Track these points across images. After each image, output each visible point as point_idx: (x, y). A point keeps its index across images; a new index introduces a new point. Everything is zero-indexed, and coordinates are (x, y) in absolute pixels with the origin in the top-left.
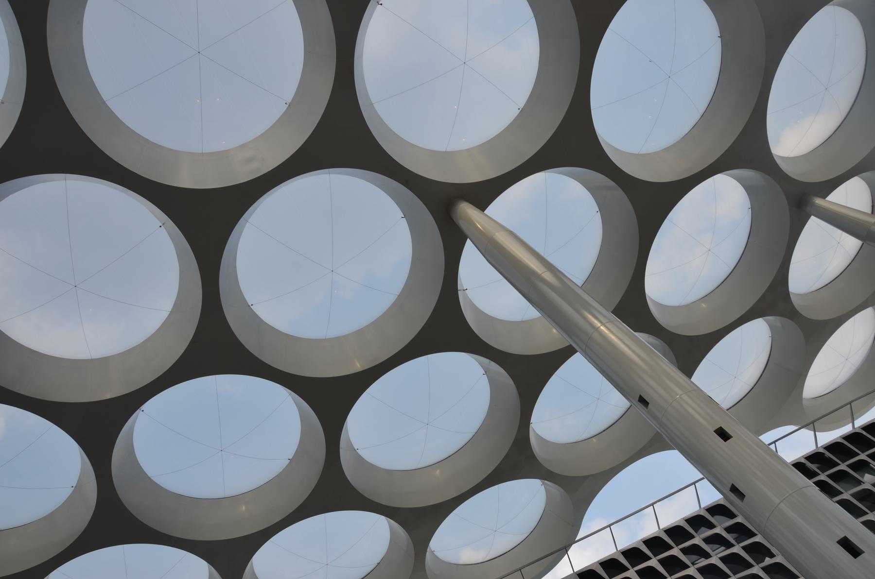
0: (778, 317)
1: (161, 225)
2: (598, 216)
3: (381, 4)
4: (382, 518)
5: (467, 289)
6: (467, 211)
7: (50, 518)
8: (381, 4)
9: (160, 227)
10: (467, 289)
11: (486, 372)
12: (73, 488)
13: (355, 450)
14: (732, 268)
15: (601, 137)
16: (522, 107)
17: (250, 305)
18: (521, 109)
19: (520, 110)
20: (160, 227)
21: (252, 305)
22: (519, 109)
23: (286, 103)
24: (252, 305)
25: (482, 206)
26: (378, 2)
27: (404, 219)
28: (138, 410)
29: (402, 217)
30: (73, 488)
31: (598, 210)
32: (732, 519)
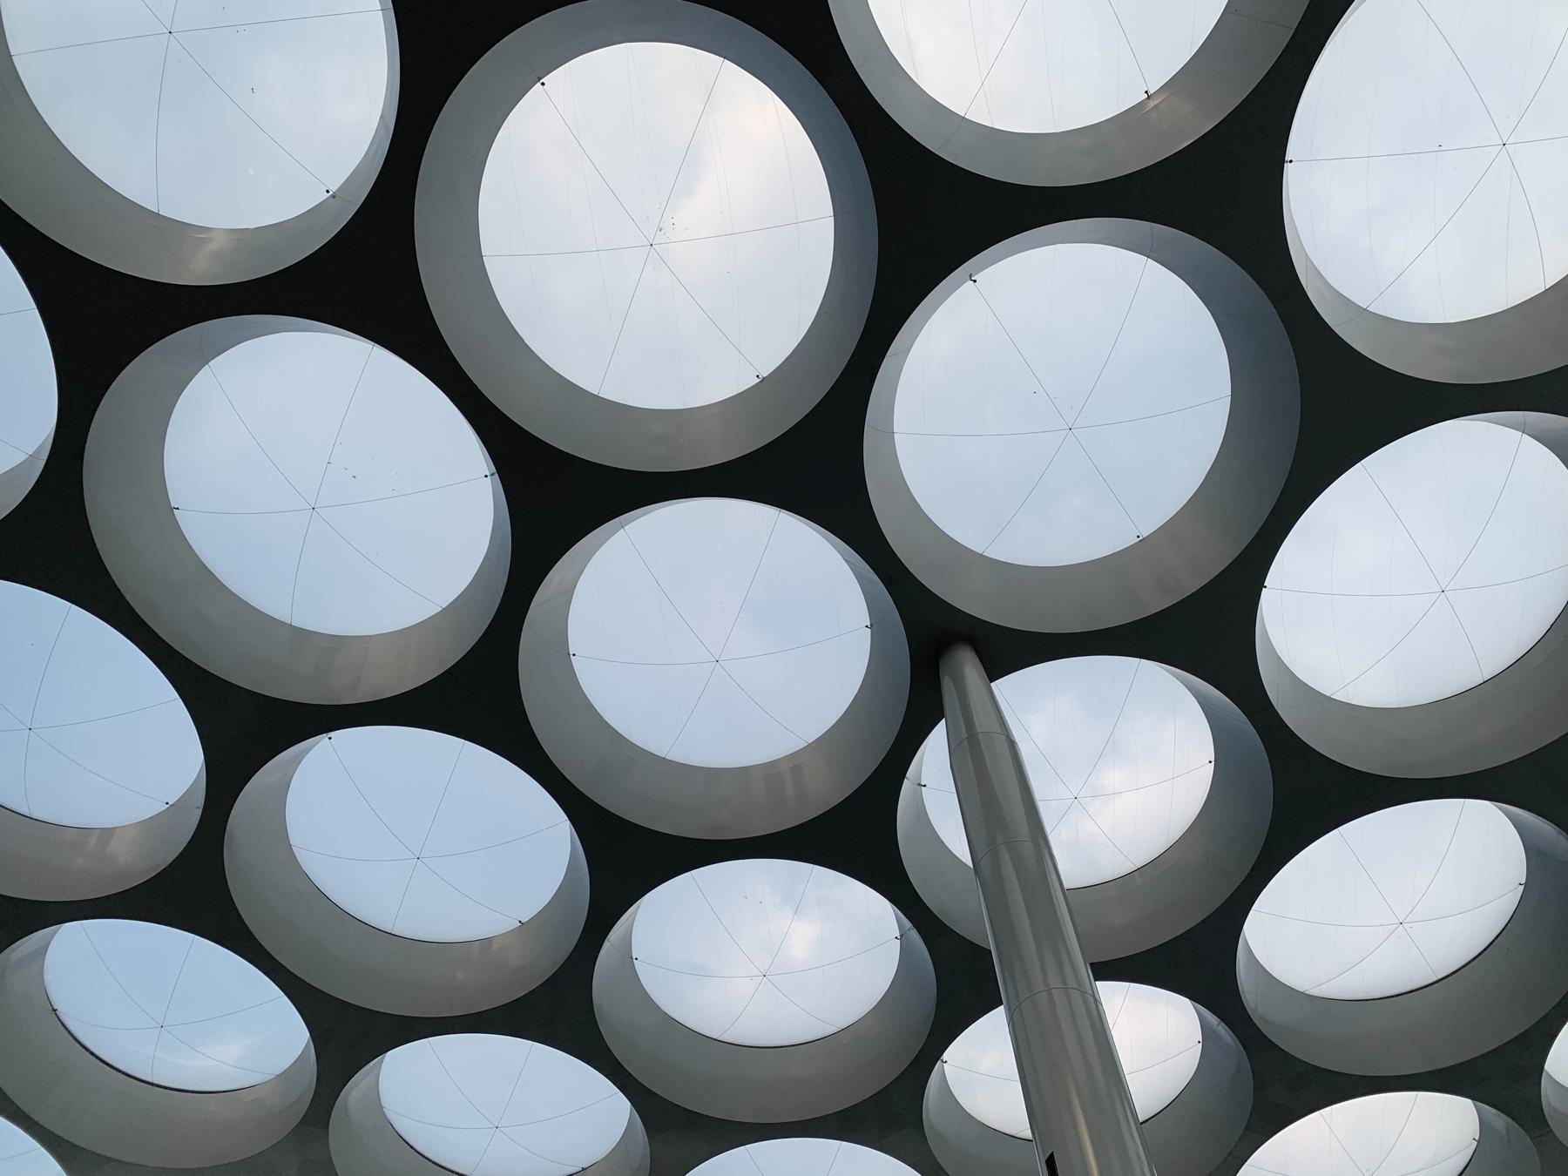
0: (1503, 1115)
1: (488, 474)
2: (1210, 769)
3: (975, 281)
4: (626, 1104)
5: (925, 786)
6: (968, 665)
7: (742, 774)
8: (975, 281)
9: (486, 476)
10: (925, 786)
11: (902, 936)
12: (168, 806)
13: (632, 958)
14: (1440, 977)
15: (19, 946)
16: (1144, 536)
17: (571, 653)
18: (1141, 538)
19: (1139, 539)
20: (486, 476)
21: (574, 655)
22: (1138, 537)
23: (758, 376)
24: (574, 655)
25: (996, 669)
26: (971, 276)
27: (869, 630)
28: (325, 735)
29: (867, 626)
30: (168, 806)
31: (1213, 759)
32: (1046, 1162)
